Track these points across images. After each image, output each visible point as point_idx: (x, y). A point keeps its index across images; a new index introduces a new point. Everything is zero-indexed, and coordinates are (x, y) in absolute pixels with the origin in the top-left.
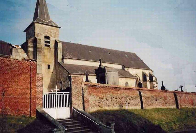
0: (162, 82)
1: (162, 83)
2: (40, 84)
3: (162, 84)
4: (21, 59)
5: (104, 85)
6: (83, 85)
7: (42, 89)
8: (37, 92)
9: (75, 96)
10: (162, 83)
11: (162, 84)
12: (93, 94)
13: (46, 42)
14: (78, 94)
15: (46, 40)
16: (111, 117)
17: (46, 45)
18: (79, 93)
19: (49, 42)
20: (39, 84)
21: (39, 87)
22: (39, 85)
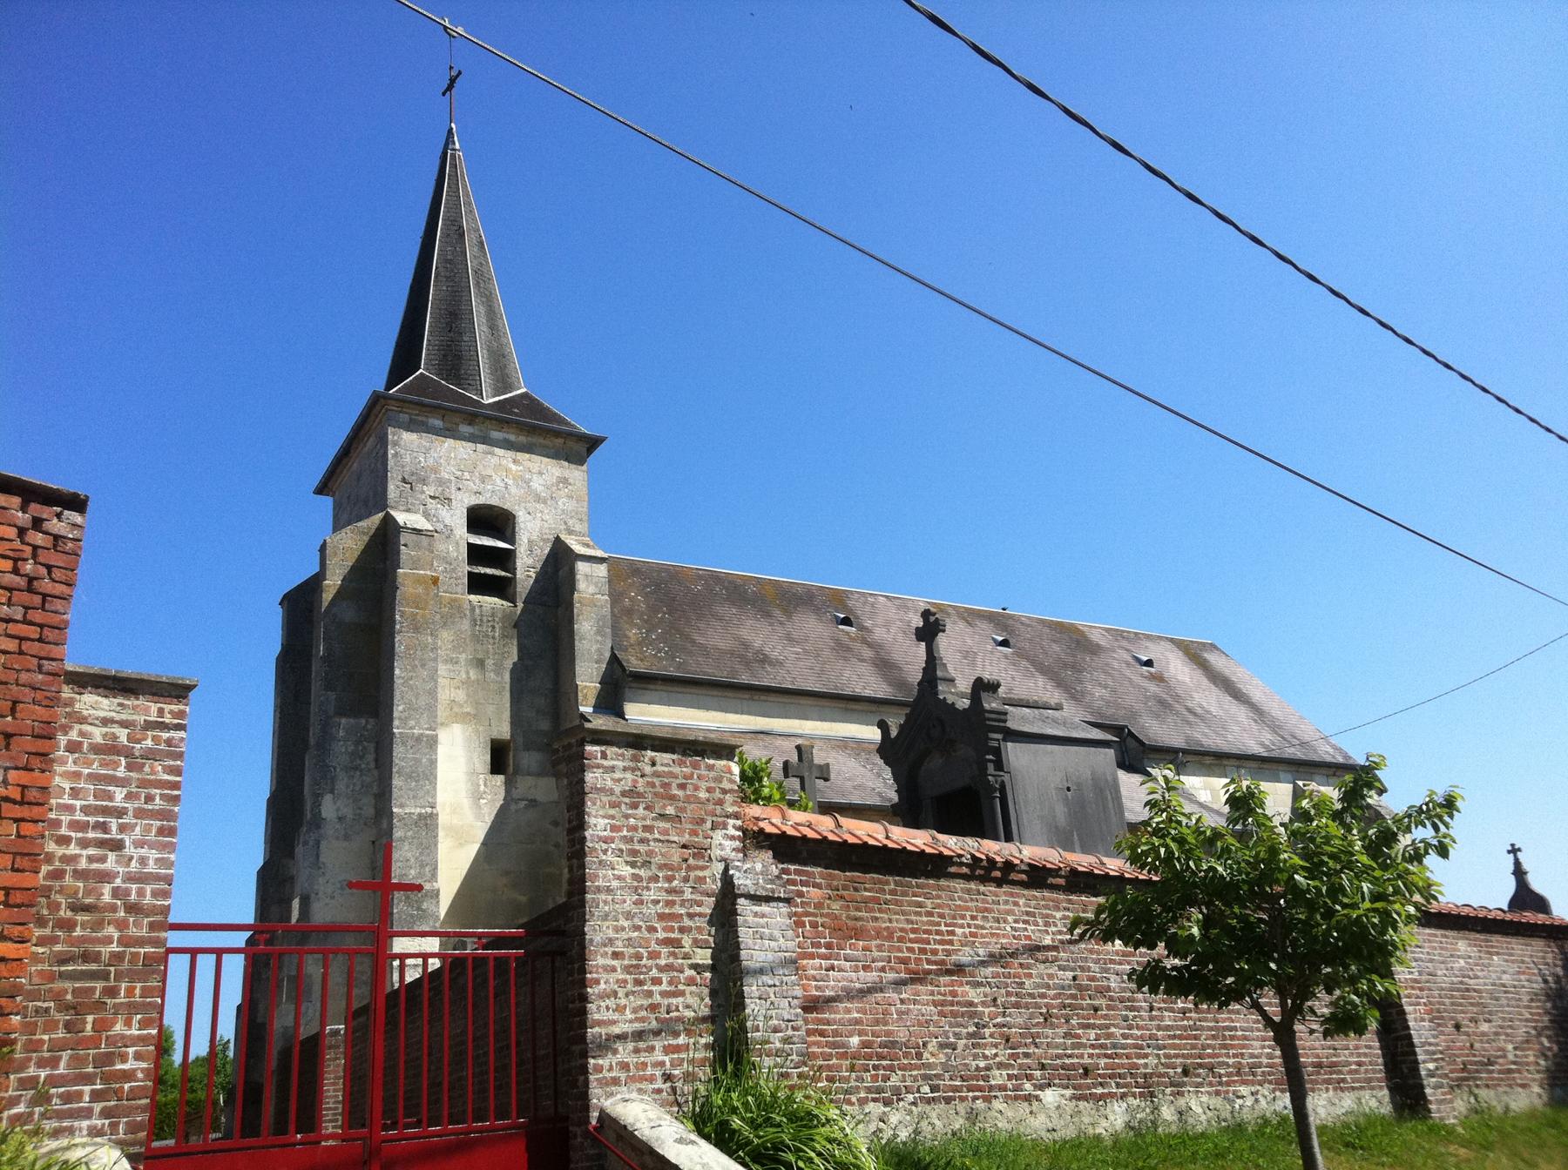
0: (1514, 850)
1: (1517, 864)
2: (139, 814)
3: (1519, 873)
4: (332, 696)
5: (991, 848)
6: (728, 844)
7: (157, 878)
8: (603, 897)
9: (627, 969)
10: (1517, 864)
11: (1519, 873)
12: (1200, 1129)
13: (475, 553)
14: (665, 950)
15: (471, 541)
16: (856, 1015)
17: (478, 584)
18: (682, 930)
19: (504, 559)
20: (120, 813)
21: (117, 846)
22: (114, 824)
